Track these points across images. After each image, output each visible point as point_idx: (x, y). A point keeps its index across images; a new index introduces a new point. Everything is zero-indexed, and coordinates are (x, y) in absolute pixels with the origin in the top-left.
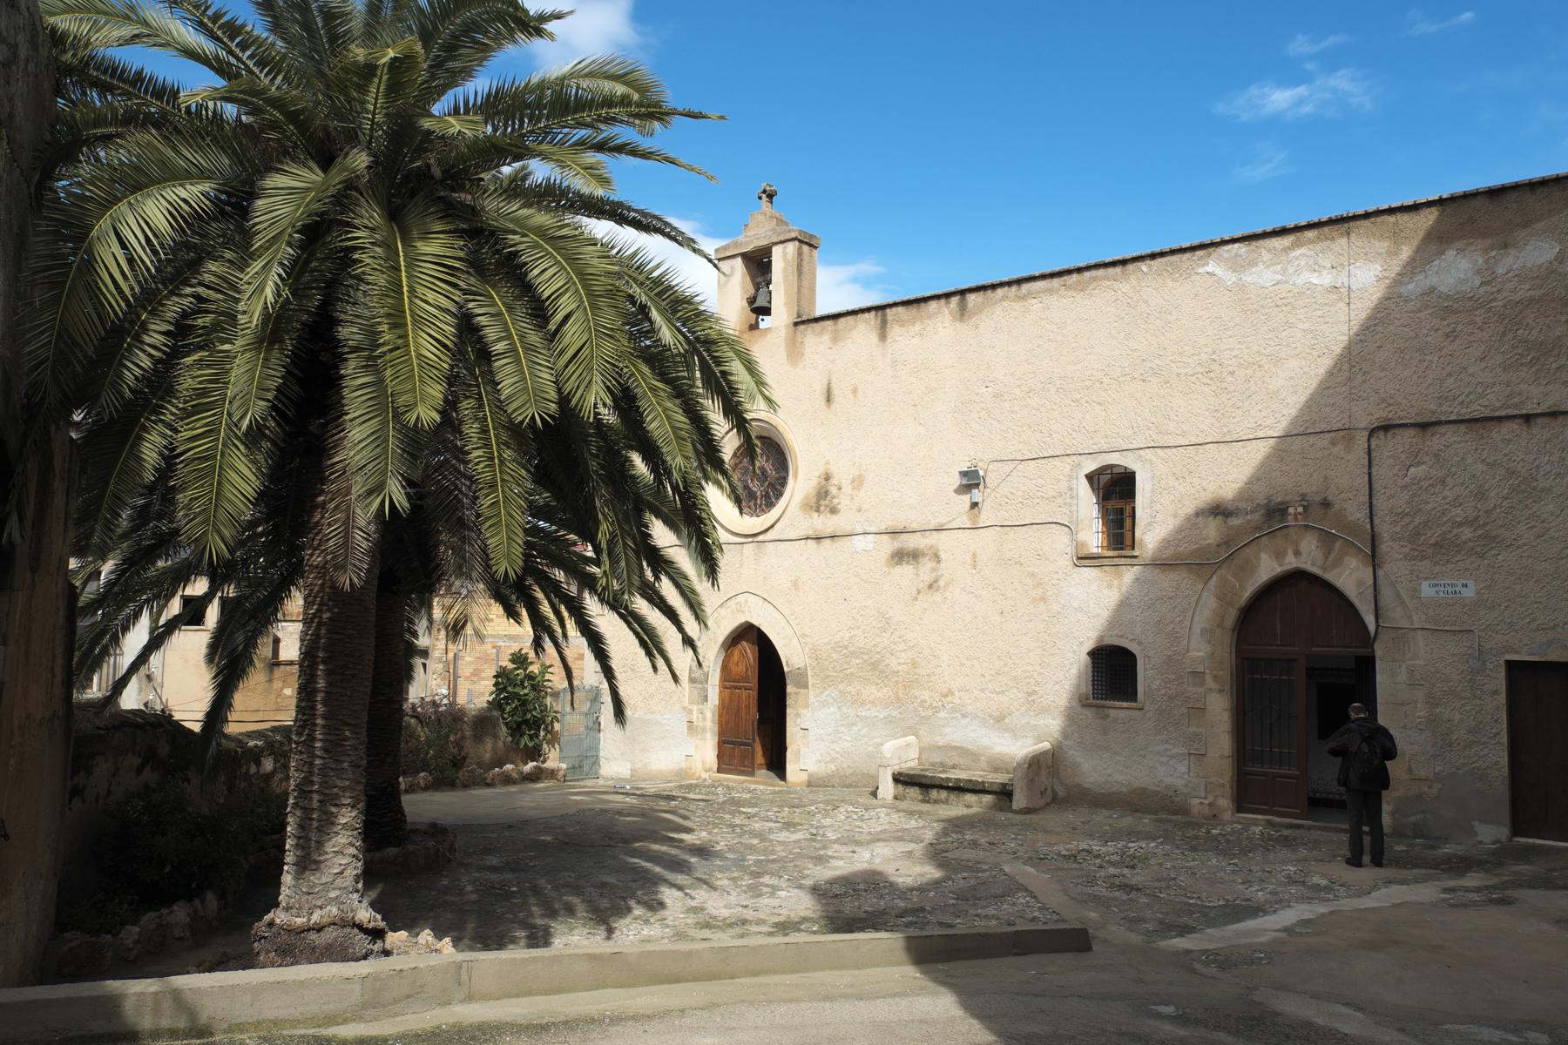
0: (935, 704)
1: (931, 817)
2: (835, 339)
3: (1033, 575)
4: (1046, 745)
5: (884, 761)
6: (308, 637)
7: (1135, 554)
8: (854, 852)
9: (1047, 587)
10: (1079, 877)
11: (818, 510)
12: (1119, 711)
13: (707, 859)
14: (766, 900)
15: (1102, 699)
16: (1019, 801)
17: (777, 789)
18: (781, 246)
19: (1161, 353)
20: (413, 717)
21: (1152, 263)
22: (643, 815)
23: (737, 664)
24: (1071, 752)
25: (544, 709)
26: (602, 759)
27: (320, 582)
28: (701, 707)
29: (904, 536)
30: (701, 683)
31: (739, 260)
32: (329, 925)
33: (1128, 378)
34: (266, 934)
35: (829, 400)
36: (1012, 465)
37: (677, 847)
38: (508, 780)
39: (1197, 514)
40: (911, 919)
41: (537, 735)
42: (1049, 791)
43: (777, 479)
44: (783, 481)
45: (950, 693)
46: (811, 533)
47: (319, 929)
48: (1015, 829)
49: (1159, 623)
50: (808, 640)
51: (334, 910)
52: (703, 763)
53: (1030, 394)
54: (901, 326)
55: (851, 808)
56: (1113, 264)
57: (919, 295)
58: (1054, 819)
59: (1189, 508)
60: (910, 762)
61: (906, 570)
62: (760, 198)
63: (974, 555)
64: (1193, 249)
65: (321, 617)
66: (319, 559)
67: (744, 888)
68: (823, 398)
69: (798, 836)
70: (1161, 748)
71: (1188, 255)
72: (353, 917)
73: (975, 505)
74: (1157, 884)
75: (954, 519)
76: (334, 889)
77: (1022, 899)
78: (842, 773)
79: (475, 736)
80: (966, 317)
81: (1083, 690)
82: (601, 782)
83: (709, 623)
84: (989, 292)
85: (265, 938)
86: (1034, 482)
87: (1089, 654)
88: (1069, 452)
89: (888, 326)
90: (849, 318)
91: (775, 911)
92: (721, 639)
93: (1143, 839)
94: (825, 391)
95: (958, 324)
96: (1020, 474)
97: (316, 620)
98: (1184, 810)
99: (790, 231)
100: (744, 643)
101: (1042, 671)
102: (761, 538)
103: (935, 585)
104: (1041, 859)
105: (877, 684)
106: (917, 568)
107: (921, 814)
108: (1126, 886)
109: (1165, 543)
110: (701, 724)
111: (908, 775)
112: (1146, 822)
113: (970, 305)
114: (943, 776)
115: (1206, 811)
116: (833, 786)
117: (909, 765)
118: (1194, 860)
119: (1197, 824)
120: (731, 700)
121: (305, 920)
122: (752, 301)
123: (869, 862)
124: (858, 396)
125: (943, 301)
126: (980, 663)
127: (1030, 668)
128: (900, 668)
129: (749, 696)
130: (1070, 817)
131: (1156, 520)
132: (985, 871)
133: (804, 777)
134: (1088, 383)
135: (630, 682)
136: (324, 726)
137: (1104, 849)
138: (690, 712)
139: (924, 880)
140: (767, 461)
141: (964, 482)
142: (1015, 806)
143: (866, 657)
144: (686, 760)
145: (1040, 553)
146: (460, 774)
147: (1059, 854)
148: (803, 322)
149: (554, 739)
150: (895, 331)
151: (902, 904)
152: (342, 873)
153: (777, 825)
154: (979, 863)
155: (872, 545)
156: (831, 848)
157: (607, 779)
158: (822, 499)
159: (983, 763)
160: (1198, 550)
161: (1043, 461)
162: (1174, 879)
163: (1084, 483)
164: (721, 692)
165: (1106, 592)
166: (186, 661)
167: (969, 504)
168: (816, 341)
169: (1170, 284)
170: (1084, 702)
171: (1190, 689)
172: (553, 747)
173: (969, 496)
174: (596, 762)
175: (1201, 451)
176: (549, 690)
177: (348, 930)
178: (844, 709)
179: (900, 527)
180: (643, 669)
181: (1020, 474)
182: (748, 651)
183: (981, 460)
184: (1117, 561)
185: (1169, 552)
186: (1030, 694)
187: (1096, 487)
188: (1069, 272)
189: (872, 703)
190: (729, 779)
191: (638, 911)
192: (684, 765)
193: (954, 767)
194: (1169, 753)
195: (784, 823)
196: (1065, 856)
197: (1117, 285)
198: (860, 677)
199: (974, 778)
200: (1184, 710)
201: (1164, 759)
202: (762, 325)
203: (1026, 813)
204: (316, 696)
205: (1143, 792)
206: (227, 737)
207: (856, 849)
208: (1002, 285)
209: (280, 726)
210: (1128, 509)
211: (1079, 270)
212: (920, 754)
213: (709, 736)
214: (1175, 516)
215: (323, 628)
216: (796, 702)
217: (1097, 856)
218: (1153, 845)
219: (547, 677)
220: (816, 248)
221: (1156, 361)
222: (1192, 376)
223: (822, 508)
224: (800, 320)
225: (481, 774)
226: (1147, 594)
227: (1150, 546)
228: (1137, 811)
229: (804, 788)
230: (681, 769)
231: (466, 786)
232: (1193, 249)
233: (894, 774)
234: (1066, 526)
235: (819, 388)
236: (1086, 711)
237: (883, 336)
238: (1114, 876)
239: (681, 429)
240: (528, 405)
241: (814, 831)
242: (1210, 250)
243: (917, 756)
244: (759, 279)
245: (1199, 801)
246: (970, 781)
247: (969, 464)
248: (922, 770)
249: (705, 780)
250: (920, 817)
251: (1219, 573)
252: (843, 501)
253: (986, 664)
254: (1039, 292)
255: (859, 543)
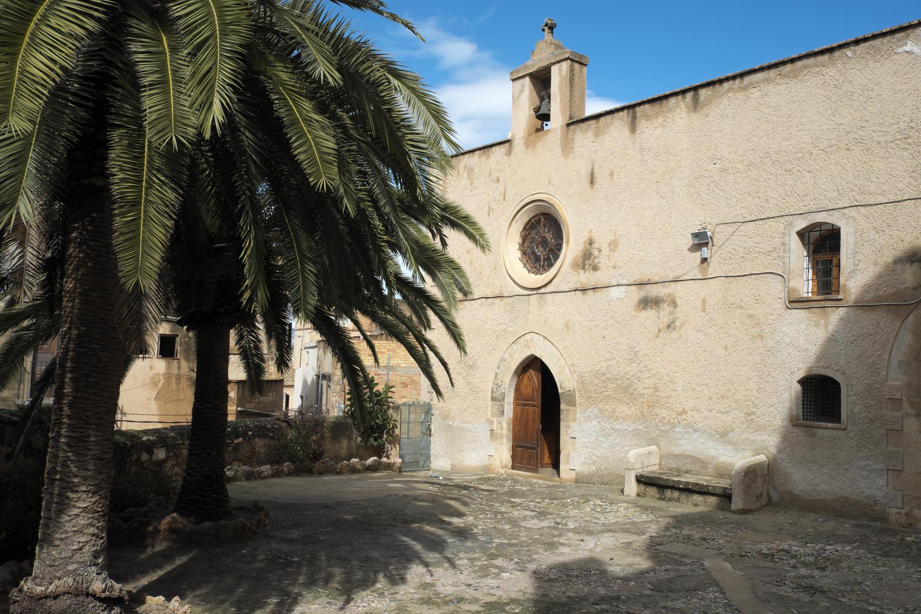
0: (672, 421)
1: (660, 513)
2: (597, 135)
3: (751, 316)
4: (762, 458)
5: (629, 465)
6: (61, 351)
7: (840, 297)
8: (582, 540)
9: (764, 326)
10: (770, 576)
11: (584, 268)
12: (825, 431)
13: (461, 540)
14: (490, 581)
15: (811, 420)
16: (737, 503)
17: (552, 483)
18: (558, 65)
19: (863, 125)
20: (284, 421)
21: (856, 48)
22: (433, 502)
23: (526, 387)
24: (784, 464)
25: (386, 419)
26: (432, 456)
27: (70, 305)
28: (499, 419)
29: (648, 286)
30: (500, 401)
31: (527, 79)
32: (64, 594)
33: (834, 148)
34: (19, 598)
35: (592, 182)
36: (735, 226)
37: (443, 529)
38: (353, 470)
39: (895, 262)
40: (604, 607)
41: (381, 438)
42: (765, 495)
43: (556, 245)
44: (559, 247)
45: (684, 412)
46: (578, 286)
47: (56, 597)
48: (728, 527)
49: (860, 356)
50: (576, 368)
51: (70, 581)
52: (501, 461)
53: (750, 168)
54: (647, 120)
55: (599, 502)
56: (822, 52)
57: (661, 94)
58: (765, 520)
59: (888, 257)
60: (652, 467)
61: (650, 313)
62: (543, 30)
63: (704, 301)
64: (892, 32)
65: (70, 334)
66: (71, 286)
67: (476, 568)
68: (588, 181)
69: (545, 524)
70: (862, 463)
71: (888, 38)
72: (88, 588)
73: (704, 260)
74: (842, 588)
75: (688, 272)
76: (73, 563)
77: (712, 594)
78: (601, 473)
79: (333, 436)
80: (698, 108)
81: (795, 413)
82: (430, 473)
83: (467, 350)
84: (717, 86)
85: (18, 601)
86: (753, 239)
87: (799, 382)
88: (782, 214)
89: (637, 120)
90: (608, 117)
91: (492, 591)
92: (514, 367)
93: (841, 542)
94: (589, 176)
95: (692, 115)
96: (742, 234)
97: (67, 337)
98: (882, 518)
99: (564, 53)
100: (531, 371)
101: (759, 395)
102: (542, 290)
103: (673, 325)
104: (742, 556)
105: (628, 404)
106: (658, 312)
107: (653, 510)
108: (812, 587)
109: (867, 288)
110: (499, 432)
111: (647, 477)
112: (847, 527)
113: (702, 98)
114: (675, 479)
115: (903, 519)
116: (594, 483)
117: (650, 469)
118: (884, 565)
119: (893, 530)
120: (522, 414)
121: (43, 588)
122: (537, 110)
123: (591, 550)
124: (615, 178)
125: (680, 97)
126: (708, 388)
127: (749, 393)
128: (645, 391)
129: (535, 412)
130: (781, 518)
131: (859, 268)
132: (687, 564)
133: (573, 475)
134: (800, 155)
135: (451, 400)
136: (69, 425)
137: (802, 550)
138: (492, 422)
139: (630, 570)
140: (549, 232)
141: (696, 242)
142: (734, 507)
143: (619, 382)
144: (489, 459)
145: (758, 298)
146: (316, 465)
147: (760, 553)
148: (573, 123)
149: (395, 440)
150: (642, 124)
151: (602, 591)
152: (81, 549)
153: (533, 514)
154: (685, 556)
155: (624, 294)
156: (565, 535)
157: (435, 471)
158: (587, 260)
159: (711, 469)
160: (896, 293)
161: (761, 222)
162: (860, 583)
163: (795, 240)
164: (514, 408)
165: (814, 330)
166: (136, 379)
167: (699, 260)
168: (583, 137)
169: (872, 65)
170: (794, 422)
171: (889, 413)
172: (395, 446)
173: (699, 253)
174: (428, 458)
175: (899, 207)
176: (391, 405)
177: (81, 598)
178: (602, 422)
179: (645, 279)
180: (459, 390)
181: (742, 234)
182: (534, 377)
183: (710, 224)
184: (823, 304)
185: (869, 296)
186: (749, 415)
187: (806, 242)
188: (784, 63)
189: (624, 418)
190: (519, 475)
191: (300, 598)
192: (486, 463)
193: (687, 472)
194: (870, 468)
195: (539, 513)
196: (765, 554)
197: (825, 70)
198: (614, 398)
199: (700, 482)
200: (882, 431)
201: (865, 473)
202: (546, 128)
203: (742, 513)
204: (63, 399)
205: (846, 501)
206: (120, 432)
207: (586, 538)
208: (727, 79)
209: (176, 426)
210: (835, 260)
211: (792, 61)
212: (660, 461)
213: (505, 441)
214: (875, 264)
215: (72, 343)
216: (567, 417)
217: (793, 557)
218: (848, 548)
219: (390, 394)
220: (585, 65)
221: (859, 132)
222: (892, 142)
223: (587, 267)
224: (571, 121)
225: (332, 465)
226: (850, 332)
227: (853, 290)
228: (841, 516)
229: (573, 484)
230: (485, 466)
231: (321, 473)
232: (892, 32)
233: (636, 476)
234: (779, 275)
235: (585, 172)
236: (796, 430)
237: (633, 129)
238: (804, 577)
239: (329, 154)
240: (168, 130)
241: (559, 520)
242: (908, 32)
243: (658, 462)
244: (543, 93)
245: (896, 510)
246: (697, 484)
247: (700, 227)
248: (660, 474)
249: (502, 474)
250: (652, 513)
251: (915, 312)
252: (602, 261)
253: (713, 389)
254: (758, 83)
255: (615, 293)
